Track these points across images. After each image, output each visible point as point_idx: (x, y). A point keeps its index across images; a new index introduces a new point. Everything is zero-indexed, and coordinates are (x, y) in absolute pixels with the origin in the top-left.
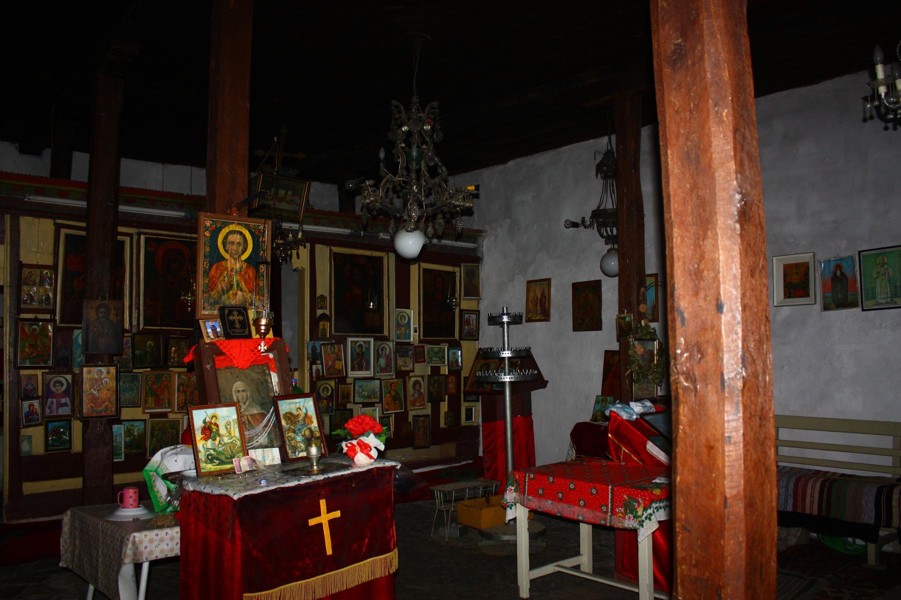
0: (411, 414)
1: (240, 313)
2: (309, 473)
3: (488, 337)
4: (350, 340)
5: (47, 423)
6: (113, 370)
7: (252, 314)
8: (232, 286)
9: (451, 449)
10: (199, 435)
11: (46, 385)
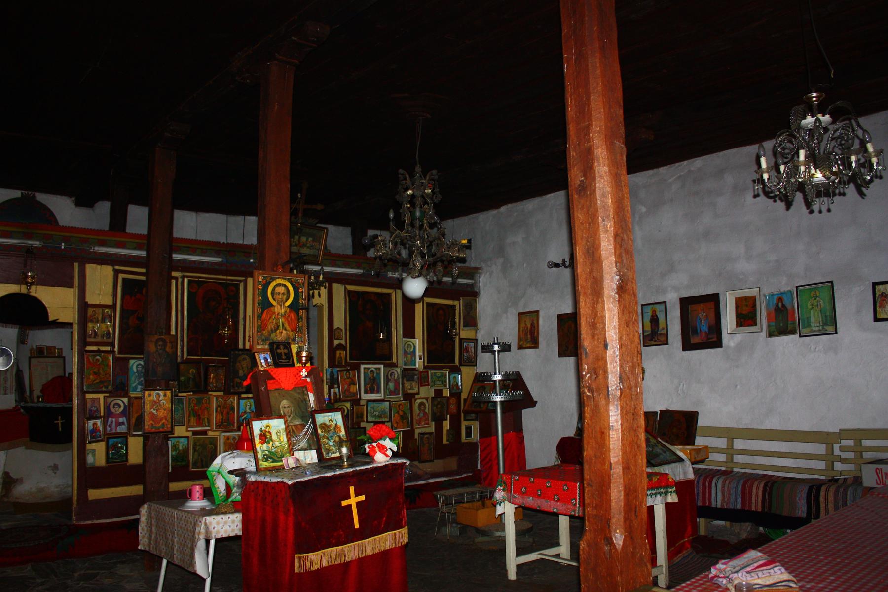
0: (417, 432)
1: (285, 347)
2: (341, 467)
3: (484, 363)
4: (363, 366)
5: (108, 438)
6: (169, 393)
7: (294, 349)
8: (278, 327)
9: (452, 463)
10: (257, 441)
11: (107, 407)
